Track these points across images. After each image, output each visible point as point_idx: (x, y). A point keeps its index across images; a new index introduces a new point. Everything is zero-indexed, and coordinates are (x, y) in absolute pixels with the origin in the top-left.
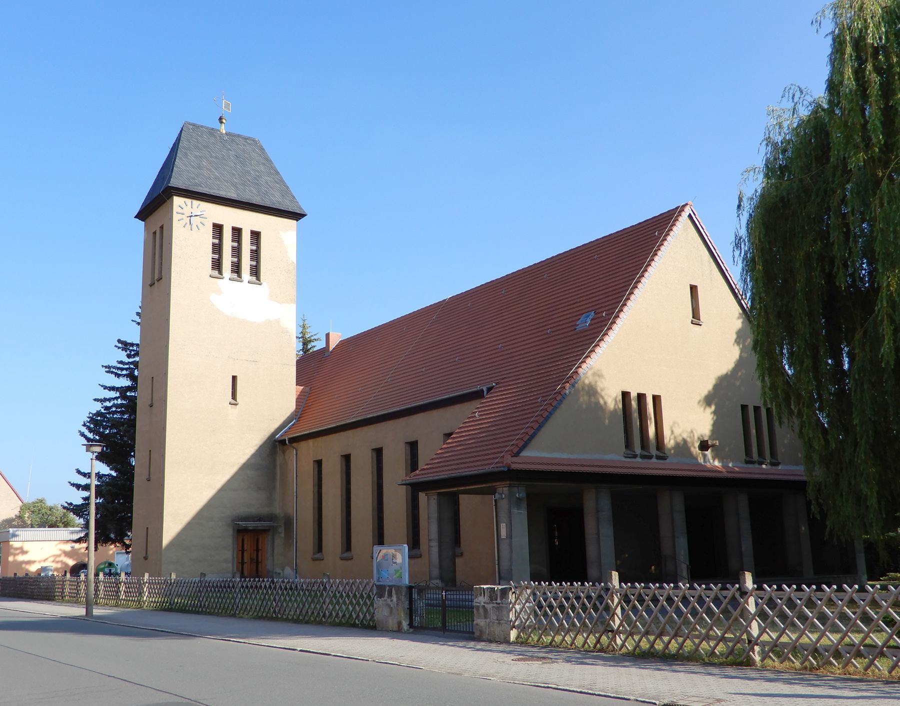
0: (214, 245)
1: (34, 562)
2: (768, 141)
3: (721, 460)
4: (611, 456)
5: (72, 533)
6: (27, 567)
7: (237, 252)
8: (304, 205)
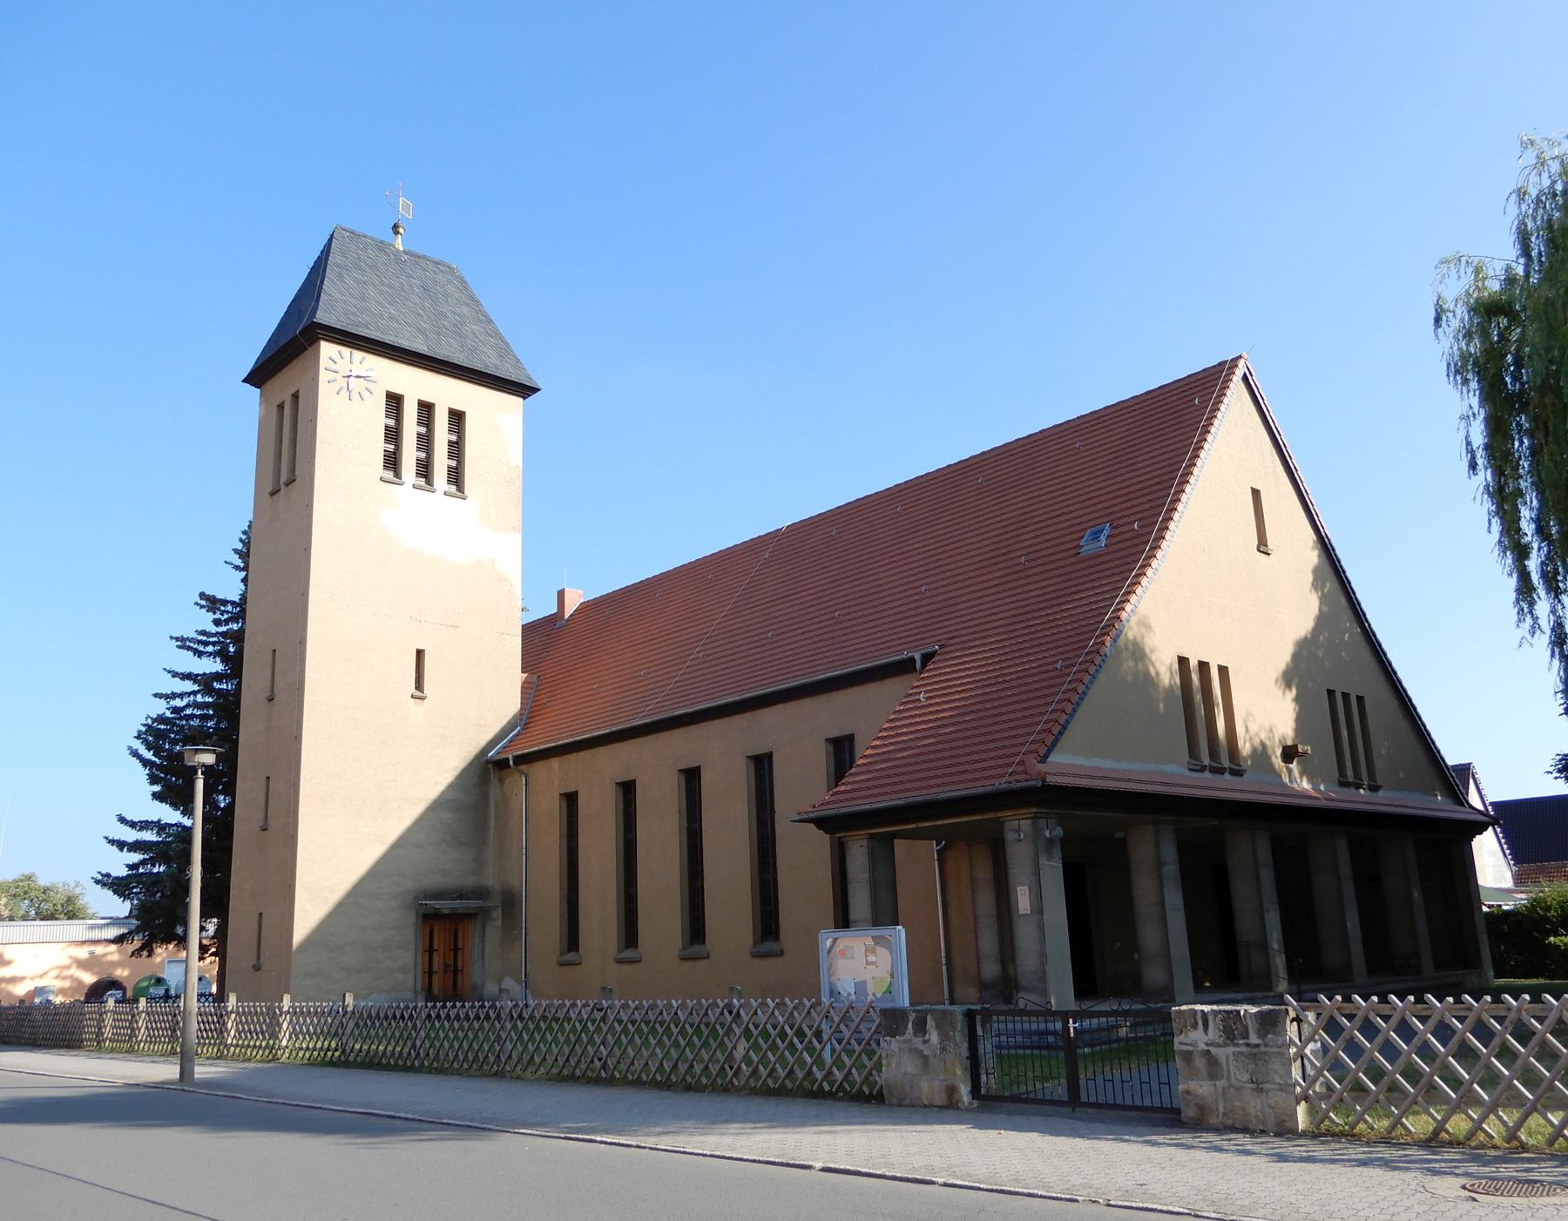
0: (387, 428)
1: (22, 979)
2: (1521, 194)
3: (1310, 781)
4: (1168, 771)
5: (92, 927)
7: (426, 442)
8: (535, 377)
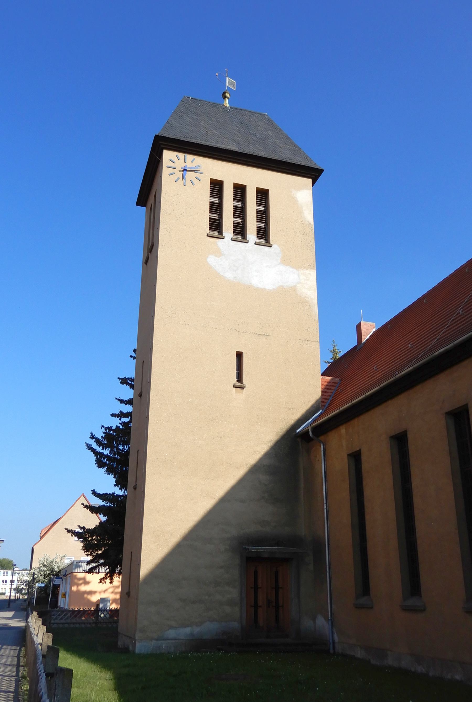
1: (95, 592)
6: (89, 597)
7: (240, 212)
8: (317, 164)
